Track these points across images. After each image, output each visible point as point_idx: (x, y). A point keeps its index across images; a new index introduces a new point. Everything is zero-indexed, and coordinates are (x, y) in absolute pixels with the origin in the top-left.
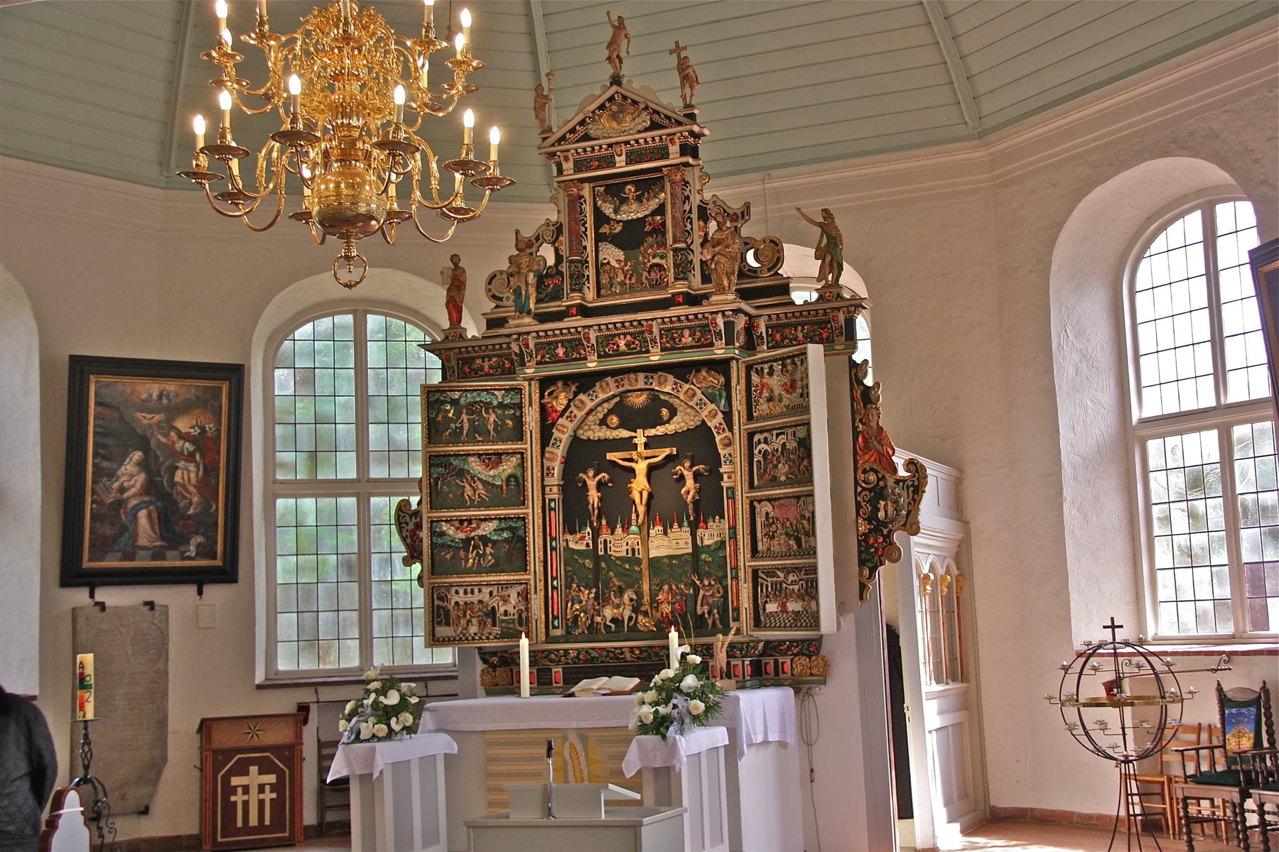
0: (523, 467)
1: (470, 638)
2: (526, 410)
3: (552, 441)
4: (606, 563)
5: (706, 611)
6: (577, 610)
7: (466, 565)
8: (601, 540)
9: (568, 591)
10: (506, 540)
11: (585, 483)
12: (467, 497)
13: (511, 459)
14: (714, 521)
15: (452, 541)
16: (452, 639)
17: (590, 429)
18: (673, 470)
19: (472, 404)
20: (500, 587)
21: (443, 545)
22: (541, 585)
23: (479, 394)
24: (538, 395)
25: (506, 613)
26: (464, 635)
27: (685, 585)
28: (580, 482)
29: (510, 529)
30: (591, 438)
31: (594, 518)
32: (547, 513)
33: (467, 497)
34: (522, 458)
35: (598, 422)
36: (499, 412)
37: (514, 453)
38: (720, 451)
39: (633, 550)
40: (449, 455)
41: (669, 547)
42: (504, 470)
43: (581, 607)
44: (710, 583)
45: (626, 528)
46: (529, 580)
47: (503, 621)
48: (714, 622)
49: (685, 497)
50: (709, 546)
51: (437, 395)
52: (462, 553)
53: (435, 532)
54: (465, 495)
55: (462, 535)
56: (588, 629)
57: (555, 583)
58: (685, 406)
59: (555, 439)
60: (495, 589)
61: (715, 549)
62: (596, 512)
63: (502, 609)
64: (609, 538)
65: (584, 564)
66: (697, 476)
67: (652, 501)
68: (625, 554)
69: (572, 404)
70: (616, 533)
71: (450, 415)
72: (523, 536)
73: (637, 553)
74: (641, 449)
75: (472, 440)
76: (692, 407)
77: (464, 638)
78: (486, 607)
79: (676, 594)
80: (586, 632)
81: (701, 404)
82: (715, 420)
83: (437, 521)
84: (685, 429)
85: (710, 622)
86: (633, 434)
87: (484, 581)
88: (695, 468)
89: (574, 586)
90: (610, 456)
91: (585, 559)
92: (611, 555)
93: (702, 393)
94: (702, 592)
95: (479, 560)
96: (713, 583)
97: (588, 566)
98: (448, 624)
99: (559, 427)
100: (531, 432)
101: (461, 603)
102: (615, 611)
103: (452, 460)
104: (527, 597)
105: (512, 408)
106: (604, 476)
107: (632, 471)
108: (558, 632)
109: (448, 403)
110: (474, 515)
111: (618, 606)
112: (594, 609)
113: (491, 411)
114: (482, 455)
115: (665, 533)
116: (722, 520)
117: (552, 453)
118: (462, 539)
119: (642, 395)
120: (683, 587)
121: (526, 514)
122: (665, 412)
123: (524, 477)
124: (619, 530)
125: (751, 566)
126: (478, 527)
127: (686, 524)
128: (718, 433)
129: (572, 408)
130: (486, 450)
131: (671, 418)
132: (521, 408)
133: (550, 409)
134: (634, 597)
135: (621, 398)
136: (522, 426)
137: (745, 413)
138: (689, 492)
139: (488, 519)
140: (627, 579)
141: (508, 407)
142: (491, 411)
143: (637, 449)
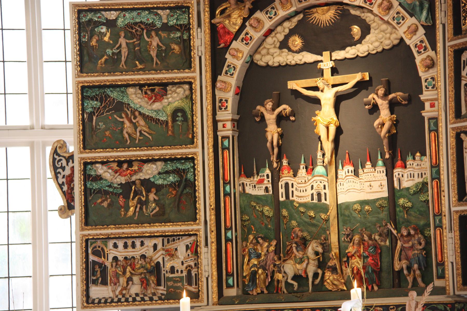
0: (192, 99)
1: (130, 299)
2: (195, 31)
3: (225, 68)
4: (288, 210)
5: (404, 266)
6: (254, 265)
7: (125, 214)
8: (282, 183)
9: (244, 244)
10: (172, 185)
11: (263, 117)
12: (126, 136)
13: (178, 90)
14: (414, 159)
15: (110, 186)
16: (109, 300)
17: (268, 54)
18: (365, 100)
19: (130, 26)
20: (166, 240)
21: (99, 191)
22: (212, 237)
23: (139, 14)
24: (207, 15)
25: (172, 270)
26: (124, 296)
27: (380, 235)
28: (257, 116)
29: (177, 172)
30: (270, 63)
31: (274, 158)
32: (220, 152)
33: (126, 136)
34: (191, 89)
35: (278, 45)
36: (163, 35)
37: (180, 83)
38: (421, 74)
39: (319, 195)
40: (105, 86)
41: (361, 190)
42: (169, 103)
43: (259, 262)
44: (409, 234)
45: (310, 169)
46: (198, 230)
47: (169, 279)
48: (415, 279)
49: (378, 130)
50: (408, 189)
51: (90, 16)
52: (121, 201)
53: (90, 176)
54: (125, 132)
55: (122, 180)
56: (267, 288)
57: (229, 234)
58: (380, 22)
59: (229, 66)
60: (159, 241)
61: (415, 193)
62: (276, 150)
63: (168, 266)
64: (291, 180)
65: (262, 212)
66: (393, 106)
67: (342, 137)
68: (309, 199)
69: (247, 24)
70: (299, 175)
71: (106, 39)
72: (192, 180)
73: (323, 198)
74: (327, 73)
75: (132, 69)
76: (388, 23)
77: (123, 300)
78: (150, 263)
79: (369, 247)
80: (265, 291)
81: (399, 19)
82: (415, 37)
83: (92, 163)
84: (380, 49)
85: (410, 279)
86: (319, 58)
87: (146, 232)
88: (391, 96)
89: (251, 237)
90: (293, 85)
91: (263, 206)
92: (294, 201)
93: (400, 4)
94: (399, 243)
95: (141, 209)
96: (412, 232)
97: (267, 213)
98: (104, 283)
99: (232, 52)
100: (200, 58)
101: (120, 258)
102: (298, 266)
103: (108, 91)
104: (196, 252)
105: (178, 30)
106: (285, 108)
107: (317, 101)
108: (232, 292)
109: (103, 24)
110: (134, 156)
111: (301, 261)
112: (275, 265)
113: (153, 34)
114: (143, 85)
115: (356, 173)
116: (424, 158)
117: (225, 82)
118: (121, 184)
119: (329, 10)
120: (377, 237)
121: (195, 154)
122: (356, 29)
123: (192, 111)
124: (302, 172)
125: (457, 212)
126: (140, 170)
127: (380, 163)
128: (419, 52)
129: (248, 29)
130: (148, 79)
131: (363, 36)
132: (189, 29)
133: (221, 31)
134: (320, 250)
135: (304, 16)
136: (190, 50)
137: (451, 26)
138: (383, 125)
139: (152, 160)
140: (313, 229)
141: (173, 28)
142: (153, 34)
143: (322, 75)
